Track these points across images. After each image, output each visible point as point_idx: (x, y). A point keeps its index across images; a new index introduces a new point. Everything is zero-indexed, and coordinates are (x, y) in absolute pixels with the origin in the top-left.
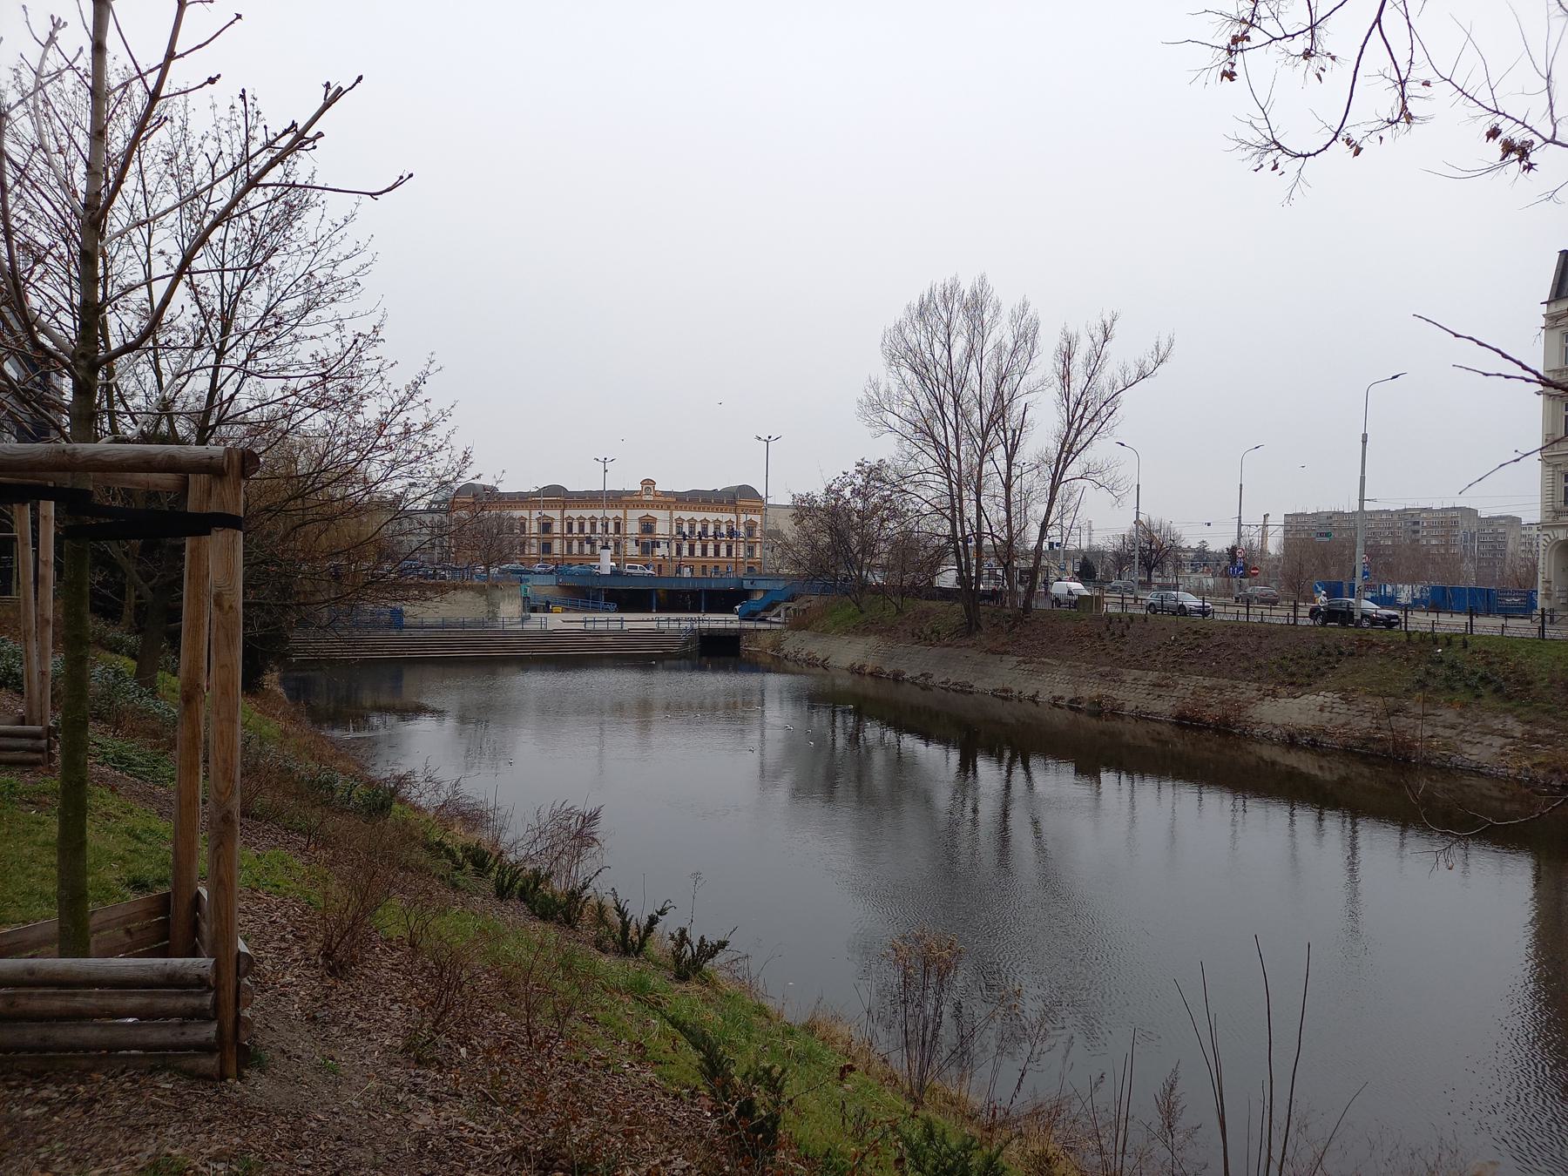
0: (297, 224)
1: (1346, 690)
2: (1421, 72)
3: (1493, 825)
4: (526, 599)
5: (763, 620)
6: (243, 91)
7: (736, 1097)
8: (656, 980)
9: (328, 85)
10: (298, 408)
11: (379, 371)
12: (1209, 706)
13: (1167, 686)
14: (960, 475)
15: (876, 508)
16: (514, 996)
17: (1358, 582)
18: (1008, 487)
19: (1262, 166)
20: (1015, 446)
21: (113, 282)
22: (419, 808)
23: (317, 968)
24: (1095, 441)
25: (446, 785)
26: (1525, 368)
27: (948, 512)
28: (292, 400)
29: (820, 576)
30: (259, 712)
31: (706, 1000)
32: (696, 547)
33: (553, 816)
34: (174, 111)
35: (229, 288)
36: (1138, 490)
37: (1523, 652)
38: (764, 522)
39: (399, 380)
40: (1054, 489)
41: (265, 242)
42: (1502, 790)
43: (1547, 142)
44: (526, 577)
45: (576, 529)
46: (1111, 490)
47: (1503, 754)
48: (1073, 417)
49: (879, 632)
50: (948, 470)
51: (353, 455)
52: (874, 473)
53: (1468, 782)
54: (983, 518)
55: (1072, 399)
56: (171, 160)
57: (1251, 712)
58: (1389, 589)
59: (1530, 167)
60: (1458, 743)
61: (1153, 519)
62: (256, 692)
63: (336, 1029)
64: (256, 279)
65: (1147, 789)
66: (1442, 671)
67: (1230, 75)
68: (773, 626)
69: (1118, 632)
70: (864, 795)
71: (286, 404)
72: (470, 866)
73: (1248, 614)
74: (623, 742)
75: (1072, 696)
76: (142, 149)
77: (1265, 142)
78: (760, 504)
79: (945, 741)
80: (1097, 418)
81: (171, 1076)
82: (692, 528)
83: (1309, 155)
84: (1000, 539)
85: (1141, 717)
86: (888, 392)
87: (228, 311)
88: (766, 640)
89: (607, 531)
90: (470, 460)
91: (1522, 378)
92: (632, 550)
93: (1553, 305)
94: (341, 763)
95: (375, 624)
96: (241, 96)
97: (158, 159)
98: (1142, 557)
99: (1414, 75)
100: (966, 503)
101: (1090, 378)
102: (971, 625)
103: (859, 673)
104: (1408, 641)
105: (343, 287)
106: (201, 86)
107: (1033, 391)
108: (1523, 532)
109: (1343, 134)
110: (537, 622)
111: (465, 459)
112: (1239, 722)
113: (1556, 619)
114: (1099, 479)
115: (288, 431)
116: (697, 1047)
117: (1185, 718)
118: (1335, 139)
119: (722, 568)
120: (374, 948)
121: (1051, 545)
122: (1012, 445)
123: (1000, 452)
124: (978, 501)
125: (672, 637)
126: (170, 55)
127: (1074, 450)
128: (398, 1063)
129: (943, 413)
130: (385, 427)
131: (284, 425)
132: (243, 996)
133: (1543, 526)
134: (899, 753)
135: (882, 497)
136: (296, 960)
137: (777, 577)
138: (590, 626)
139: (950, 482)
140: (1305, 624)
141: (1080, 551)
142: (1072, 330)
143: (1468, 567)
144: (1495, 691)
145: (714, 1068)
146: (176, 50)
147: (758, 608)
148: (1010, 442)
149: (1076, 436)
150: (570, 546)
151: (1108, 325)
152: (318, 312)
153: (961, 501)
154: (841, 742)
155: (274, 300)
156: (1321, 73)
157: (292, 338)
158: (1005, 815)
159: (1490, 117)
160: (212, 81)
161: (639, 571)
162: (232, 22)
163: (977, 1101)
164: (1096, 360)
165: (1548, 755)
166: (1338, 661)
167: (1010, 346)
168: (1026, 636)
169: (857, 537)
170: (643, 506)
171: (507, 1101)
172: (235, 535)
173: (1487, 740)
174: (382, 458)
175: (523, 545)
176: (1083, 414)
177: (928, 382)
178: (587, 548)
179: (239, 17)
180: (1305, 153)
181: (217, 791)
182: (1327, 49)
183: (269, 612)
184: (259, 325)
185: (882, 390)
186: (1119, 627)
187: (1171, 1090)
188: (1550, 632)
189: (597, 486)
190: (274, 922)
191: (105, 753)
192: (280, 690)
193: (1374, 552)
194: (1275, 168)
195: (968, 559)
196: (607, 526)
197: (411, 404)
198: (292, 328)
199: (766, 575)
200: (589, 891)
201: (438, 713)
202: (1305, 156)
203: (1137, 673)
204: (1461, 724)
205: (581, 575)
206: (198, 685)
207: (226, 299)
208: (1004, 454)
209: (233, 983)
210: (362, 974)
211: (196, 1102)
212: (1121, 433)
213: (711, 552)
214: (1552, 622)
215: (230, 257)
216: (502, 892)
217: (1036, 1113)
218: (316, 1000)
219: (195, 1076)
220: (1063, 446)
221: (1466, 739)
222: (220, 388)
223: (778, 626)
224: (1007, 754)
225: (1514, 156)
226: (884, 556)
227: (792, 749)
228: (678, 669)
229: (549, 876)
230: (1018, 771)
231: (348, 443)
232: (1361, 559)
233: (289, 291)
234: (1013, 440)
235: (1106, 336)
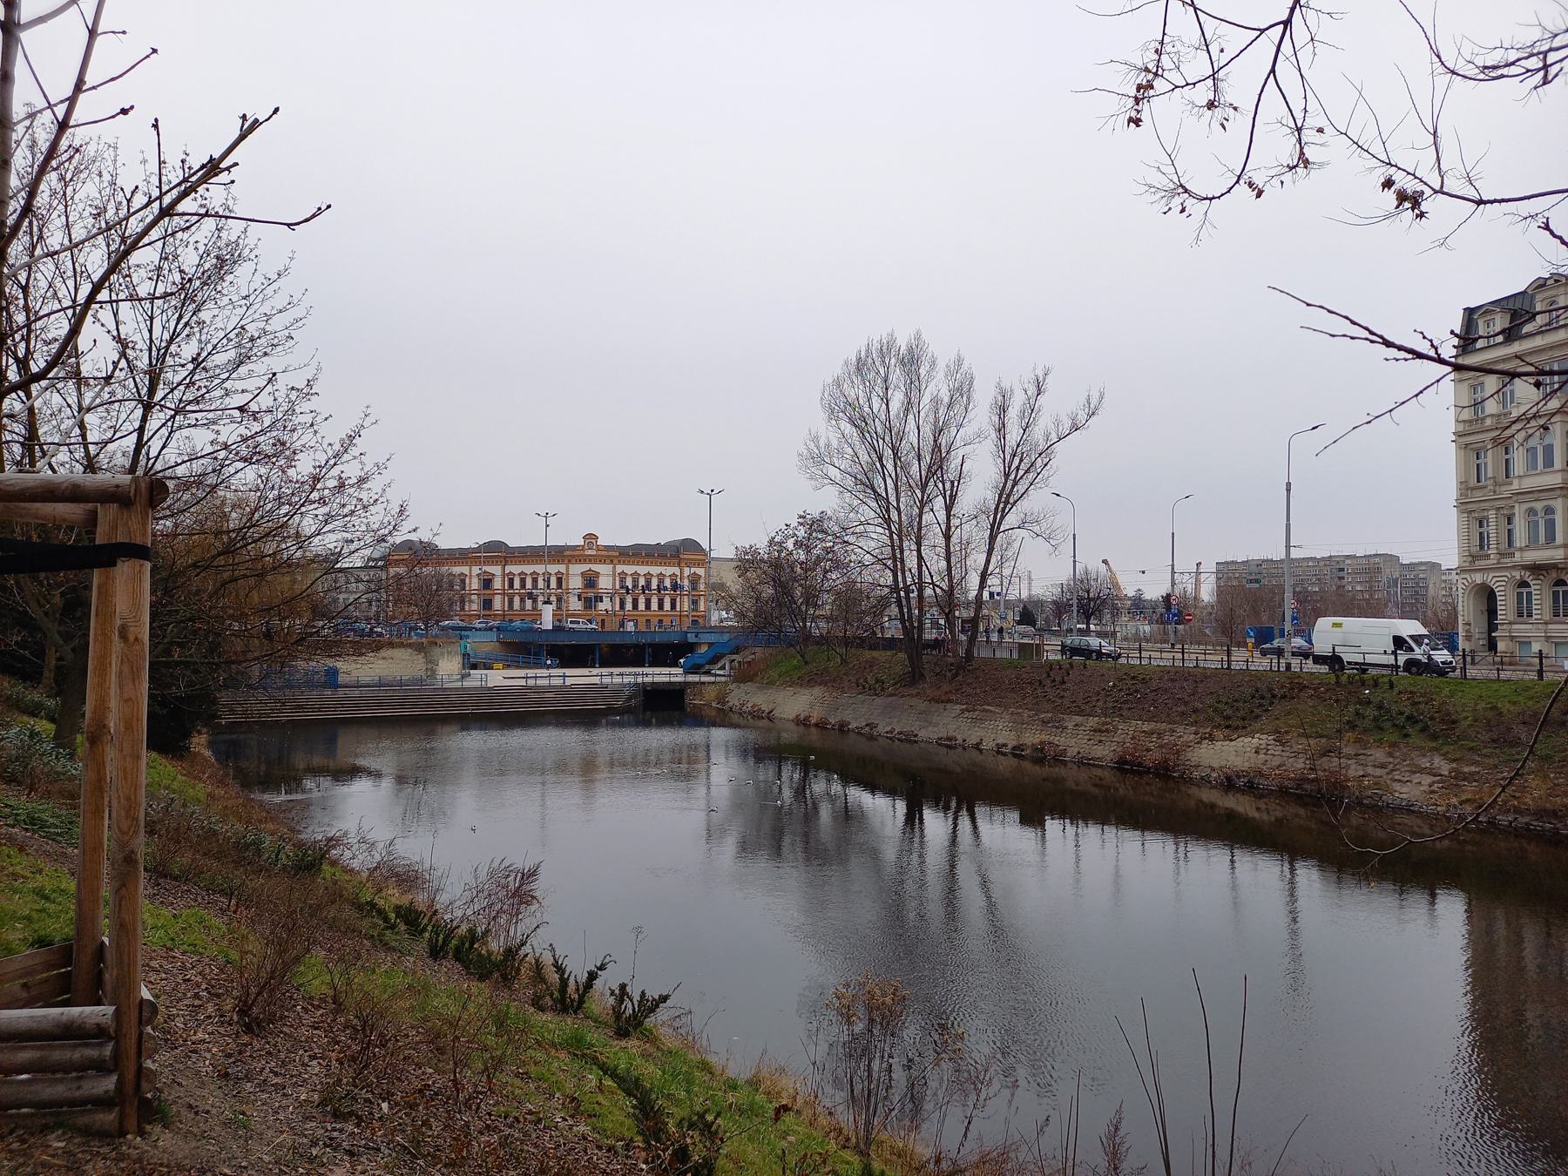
0: (229, 278)
1: (1280, 732)
2: (1314, 120)
4: (465, 656)
5: (708, 673)
6: (156, 120)
7: (669, 1143)
8: (593, 1036)
9: (244, 117)
10: (227, 462)
11: (312, 425)
12: (1148, 750)
14: (900, 525)
15: (819, 560)
17: (1288, 626)
18: (947, 537)
19: (1170, 209)
20: (953, 497)
21: (37, 337)
22: (352, 870)
23: (231, 1025)
24: (1031, 492)
25: (380, 846)
26: (1372, 333)
27: (889, 563)
28: (222, 454)
29: (765, 627)
31: (645, 1055)
32: (640, 601)
33: (491, 875)
36: (1074, 539)
38: (708, 574)
39: (333, 433)
40: (992, 538)
42: (1432, 827)
43: (1436, 192)
45: (517, 584)
47: (1432, 792)
48: (1009, 468)
50: (888, 521)
51: (285, 509)
52: (816, 525)
53: (1399, 821)
54: (924, 568)
55: (1008, 451)
56: (99, 214)
57: (1189, 755)
59: (1421, 215)
60: (1389, 782)
63: (249, 1085)
64: (186, 332)
65: (1091, 833)
66: (1370, 712)
67: (1137, 122)
68: (718, 679)
69: (1058, 679)
70: (815, 854)
71: (216, 458)
72: (403, 927)
73: (1183, 659)
74: (565, 799)
75: (1015, 743)
76: (70, 203)
77: (1173, 187)
78: (703, 557)
79: (892, 792)
80: (1032, 469)
81: (64, 1133)
82: (635, 582)
83: (1214, 198)
84: (941, 588)
85: (1083, 762)
86: (828, 445)
88: (710, 693)
89: (548, 586)
90: (407, 513)
92: (575, 605)
94: (270, 826)
97: (86, 214)
98: (1081, 606)
100: (906, 553)
101: (1025, 430)
104: (1337, 682)
105: (276, 341)
106: (113, 117)
107: (970, 444)
108: (1444, 578)
110: (477, 678)
111: (401, 512)
113: (1477, 660)
114: (1036, 529)
115: (216, 485)
116: (629, 1094)
117: (1126, 762)
118: (1237, 182)
119: (666, 621)
120: (295, 1006)
121: (991, 595)
122: (951, 496)
123: (939, 503)
124: (919, 551)
125: (617, 691)
126: (79, 87)
127: (1011, 501)
128: (314, 1117)
129: (883, 466)
130: (319, 480)
131: (212, 480)
133: (1461, 570)
134: (846, 807)
135: (825, 549)
136: (209, 1017)
138: (531, 682)
139: (891, 533)
140: (1238, 668)
141: (1020, 600)
142: (1006, 384)
144: (1423, 730)
145: (648, 1115)
146: (86, 79)
147: (702, 661)
148: (948, 493)
149: (1013, 487)
151: (1041, 379)
152: (250, 366)
153: (902, 552)
154: (787, 794)
155: (204, 354)
156: (1225, 122)
157: (223, 392)
158: (953, 866)
159: (1384, 169)
160: (124, 112)
161: (581, 626)
162: (148, 56)
163: (925, 1152)
164: (1031, 410)
165: (1474, 792)
166: (1271, 704)
167: (946, 400)
169: (800, 588)
172: (142, 565)
173: (1416, 778)
174: (315, 512)
175: (463, 602)
176: (1019, 465)
177: (867, 435)
179: (155, 51)
181: (120, 830)
183: (196, 672)
184: (188, 379)
185: (822, 444)
190: (189, 980)
191: (17, 815)
192: (207, 753)
194: (1183, 211)
195: (910, 609)
196: (549, 581)
197: (346, 457)
198: (223, 382)
200: (527, 949)
201: (376, 775)
202: (1211, 199)
203: (1078, 719)
205: (523, 631)
206: (104, 726)
207: (154, 353)
208: (943, 506)
210: (281, 1032)
211: (90, 1160)
212: (1055, 483)
213: (654, 606)
214: (1473, 663)
215: (159, 311)
216: (436, 952)
219: (88, 1133)
220: (1000, 496)
222: (146, 443)
223: (723, 679)
224: (953, 804)
225: (1407, 205)
226: (828, 607)
227: (738, 805)
228: (621, 725)
230: (965, 823)
232: (1289, 604)
233: (220, 345)
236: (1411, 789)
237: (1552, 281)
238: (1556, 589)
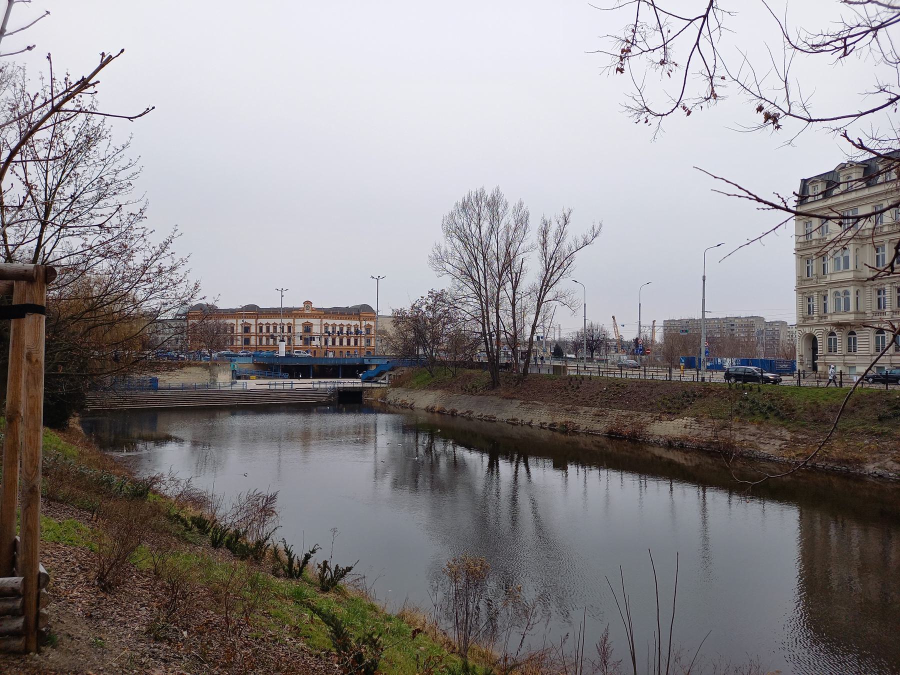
0: (93, 148)
1: (698, 416)
2: (720, 72)
3: (769, 477)
4: (234, 371)
5: (376, 382)
8: (308, 591)
9: (103, 54)
10: (92, 257)
11: (143, 236)
12: (625, 426)
13: (602, 415)
14: (487, 298)
15: (440, 317)
16: (218, 601)
18: (513, 305)
19: (639, 120)
20: (517, 282)
23: (94, 587)
24: (561, 279)
26: (750, 194)
27: (480, 319)
28: (89, 252)
30: (65, 441)
31: (338, 602)
32: (336, 340)
33: (248, 499)
34: (16, 80)
35: (50, 186)
37: (789, 393)
39: (156, 241)
40: (539, 306)
41: (73, 159)
43: (786, 114)
44: (234, 358)
45: (264, 330)
46: (570, 307)
47: (781, 449)
49: (443, 388)
50: (480, 295)
51: (126, 285)
52: (439, 297)
54: (500, 322)
55: (548, 256)
56: (14, 109)
57: (648, 429)
58: (719, 361)
59: (778, 127)
60: (757, 444)
61: (593, 323)
62: (64, 430)
63: (104, 622)
65: (594, 473)
66: (748, 405)
67: (621, 70)
68: (382, 385)
69: (576, 386)
70: (438, 487)
71: (85, 255)
72: (196, 529)
73: (645, 375)
74: (293, 454)
75: (550, 422)
79: (481, 450)
82: (334, 329)
83: (664, 115)
85: (589, 433)
86: (446, 252)
87: (49, 199)
88: (377, 394)
91: (747, 197)
92: (298, 342)
93: (799, 208)
95: (141, 387)
96: (48, 57)
97: (6, 108)
98: (588, 344)
99: (717, 73)
100: (490, 314)
101: (557, 245)
102: (494, 383)
103: (432, 412)
105: (121, 186)
106: (22, 51)
107: (526, 252)
108: (789, 330)
109: (681, 104)
110: (240, 385)
111: (196, 287)
112: (642, 435)
113: (806, 375)
114: (563, 300)
115: (85, 270)
116: (328, 624)
117: (613, 433)
118: (677, 106)
119: (352, 352)
120: (132, 576)
121: (538, 338)
122: (515, 282)
123: (509, 286)
124: (497, 313)
127: (550, 285)
128: (143, 640)
129: (477, 264)
130: (147, 268)
131: (82, 267)
132: (42, 599)
133: (798, 326)
134: (455, 457)
135: (444, 311)
136: (81, 583)
137: (384, 357)
138: (273, 387)
139: (482, 302)
141: (554, 341)
142: (547, 218)
143: (760, 349)
144: (776, 415)
145: (339, 635)
147: (373, 375)
148: (514, 280)
149: (551, 277)
150: (261, 340)
151: (567, 216)
152: (106, 201)
153: (488, 313)
155: (78, 193)
156: (670, 72)
157: (89, 215)
159: (758, 101)
160: (29, 48)
161: (302, 354)
163: (498, 654)
164: (561, 234)
166: (693, 400)
167: (513, 226)
168: (525, 389)
169: (429, 334)
170: (304, 316)
171: (211, 661)
172: (40, 317)
173: (772, 442)
174: (145, 287)
175: (232, 340)
178: (271, 341)
179: (48, 13)
180: (662, 114)
182: (673, 60)
184: (68, 208)
186: (577, 382)
187: (605, 641)
188: (803, 383)
189: (277, 305)
190: (68, 561)
192: (79, 428)
193: (711, 340)
194: (646, 122)
195: (492, 346)
196: (283, 328)
197: (163, 255)
199: (377, 356)
200: (269, 542)
202: (662, 116)
203: (587, 408)
204: (758, 433)
205: (268, 357)
206: (18, 412)
207: (48, 192)
209: (35, 593)
210: (124, 591)
213: (345, 343)
214: (804, 377)
215: (51, 168)
216: (216, 544)
217: (531, 659)
218: (93, 605)
220: (543, 282)
221: (762, 441)
222: (43, 245)
223: (385, 385)
224: (516, 456)
225: (770, 121)
226: (445, 344)
228: (326, 412)
229: (245, 532)
230: (522, 468)
231: (123, 278)
232: (704, 344)
233: (87, 188)
234: (516, 279)
235: (566, 221)
236: (770, 448)
237: (848, 165)
238: (830, 337)
